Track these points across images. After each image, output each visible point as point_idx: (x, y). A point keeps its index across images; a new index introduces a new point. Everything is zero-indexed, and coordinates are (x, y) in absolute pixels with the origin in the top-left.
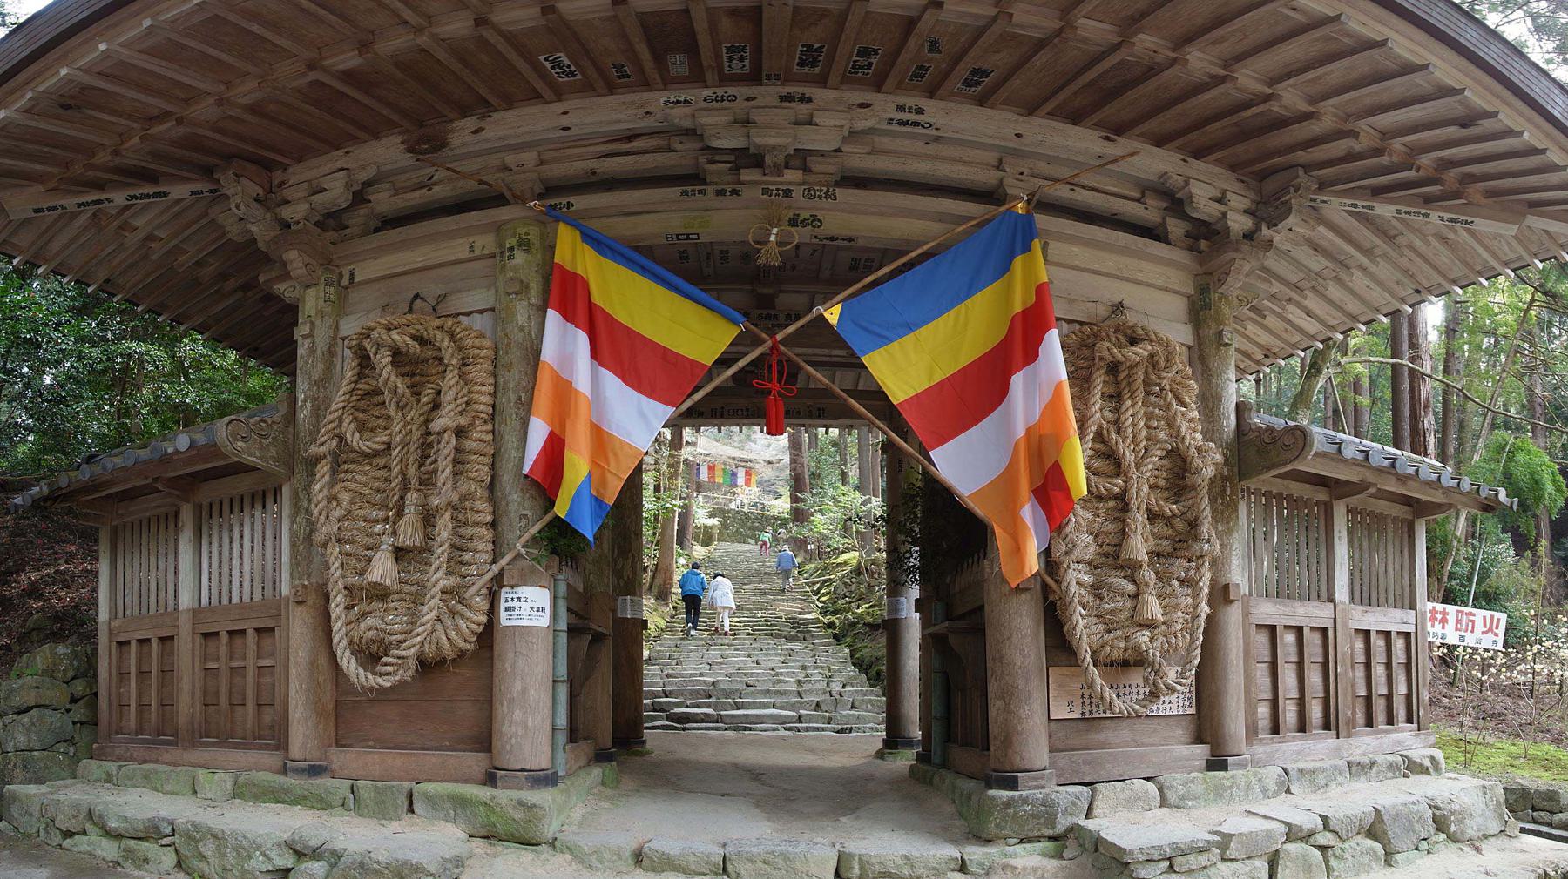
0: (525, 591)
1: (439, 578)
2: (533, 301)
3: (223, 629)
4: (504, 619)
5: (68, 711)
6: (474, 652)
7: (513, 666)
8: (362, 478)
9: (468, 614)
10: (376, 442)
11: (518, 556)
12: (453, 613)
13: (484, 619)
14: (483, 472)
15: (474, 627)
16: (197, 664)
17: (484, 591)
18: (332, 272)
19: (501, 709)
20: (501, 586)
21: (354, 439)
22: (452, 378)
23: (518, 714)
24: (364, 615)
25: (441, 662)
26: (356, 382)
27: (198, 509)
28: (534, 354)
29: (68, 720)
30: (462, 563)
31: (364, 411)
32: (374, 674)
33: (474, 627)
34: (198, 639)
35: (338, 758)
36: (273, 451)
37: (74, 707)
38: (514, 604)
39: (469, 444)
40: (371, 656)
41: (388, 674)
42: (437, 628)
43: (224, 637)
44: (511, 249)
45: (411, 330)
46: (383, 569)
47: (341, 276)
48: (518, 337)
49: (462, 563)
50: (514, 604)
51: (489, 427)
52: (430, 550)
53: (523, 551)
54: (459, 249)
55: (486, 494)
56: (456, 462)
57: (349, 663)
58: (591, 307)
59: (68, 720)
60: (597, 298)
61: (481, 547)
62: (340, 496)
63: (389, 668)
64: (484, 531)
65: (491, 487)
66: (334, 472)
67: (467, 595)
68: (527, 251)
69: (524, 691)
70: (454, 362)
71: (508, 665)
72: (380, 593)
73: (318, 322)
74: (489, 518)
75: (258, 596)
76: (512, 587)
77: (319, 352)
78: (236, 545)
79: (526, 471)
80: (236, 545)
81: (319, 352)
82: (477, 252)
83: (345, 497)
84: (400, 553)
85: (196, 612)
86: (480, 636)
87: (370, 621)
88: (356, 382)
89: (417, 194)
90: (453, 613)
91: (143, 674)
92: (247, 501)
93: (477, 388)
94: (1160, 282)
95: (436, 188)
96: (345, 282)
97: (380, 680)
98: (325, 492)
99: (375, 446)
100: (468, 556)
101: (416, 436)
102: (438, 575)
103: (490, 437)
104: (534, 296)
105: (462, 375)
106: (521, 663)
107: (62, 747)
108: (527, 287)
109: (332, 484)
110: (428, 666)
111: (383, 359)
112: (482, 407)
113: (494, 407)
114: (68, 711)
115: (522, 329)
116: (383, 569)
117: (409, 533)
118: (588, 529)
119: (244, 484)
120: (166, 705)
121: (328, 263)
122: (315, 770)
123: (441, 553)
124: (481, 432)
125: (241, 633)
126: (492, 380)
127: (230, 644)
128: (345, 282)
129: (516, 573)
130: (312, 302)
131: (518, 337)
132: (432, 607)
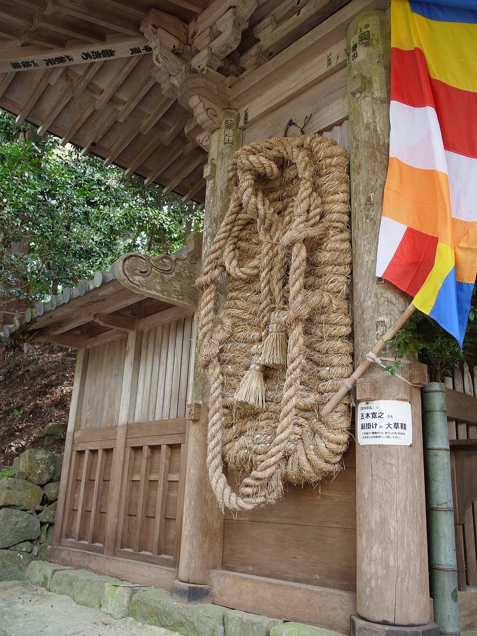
0: (382, 406)
1: (291, 394)
2: (377, 94)
3: (145, 443)
4: (363, 439)
5: (38, 512)
6: (340, 473)
7: (371, 492)
8: (242, 303)
9: (326, 433)
10: (247, 270)
11: (372, 366)
12: (315, 432)
13: (344, 437)
14: (340, 283)
15: (334, 446)
16: (126, 476)
17: (342, 408)
18: (231, 115)
19: (362, 542)
20: (358, 402)
21: (232, 267)
22: (304, 190)
23: (377, 550)
24: (241, 433)
25: (308, 485)
26: (237, 213)
27: (140, 335)
28: (381, 150)
29: (36, 520)
30: (321, 379)
31: (247, 240)
32: (238, 495)
33: (334, 446)
34: (128, 450)
35: (223, 582)
36: (177, 285)
37: (45, 508)
38: (370, 420)
39: (324, 256)
40: (234, 473)
41: (248, 496)
42: (316, 455)
43: (146, 451)
44: (355, 47)
45: (273, 153)
46: (250, 388)
47: (238, 117)
48: (364, 136)
49: (321, 379)
50: (370, 420)
51: (345, 235)
52: (284, 367)
53: (378, 360)
54: (318, 66)
55: (344, 305)
56: (308, 274)
57: (218, 482)
58: (432, 83)
59: (36, 520)
60: (436, 75)
61: (336, 360)
62: (224, 320)
63: (249, 490)
64: (339, 343)
65: (350, 297)
66: (216, 299)
67: (323, 412)
68: (367, 45)
69: (383, 522)
70: (307, 174)
71: (365, 490)
72: (248, 413)
73: (219, 164)
74: (345, 330)
75: (173, 415)
76: (367, 401)
77: (219, 192)
78: (162, 368)
79: (380, 273)
80: (162, 368)
81: (219, 192)
82: (334, 64)
83: (228, 322)
84: (268, 373)
85: (129, 427)
86: (345, 455)
87: (242, 440)
88: (237, 213)
89: (290, 21)
90: (315, 432)
91: (90, 481)
92: (173, 327)
93: (330, 198)
94: (174, 34)
95: (303, 11)
96: (241, 123)
97: (241, 502)
98: (211, 315)
99: (248, 271)
100: (324, 372)
101: (280, 256)
102: (291, 391)
103: (346, 245)
104: (378, 89)
105: (316, 188)
106: (378, 488)
107: (25, 547)
108: (370, 82)
109: (216, 310)
110: (296, 489)
111: (246, 181)
112: (335, 216)
113: (350, 214)
114: (38, 512)
115: (367, 127)
116: (250, 388)
117: (266, 359)
118: (455, 329)
119: (169, 316)
120: (100, 523)
121: (228, 107)
122: (196, 594)
123: (293, 374)
124: (335, 242)
125: (158, 448)
126: (344, 187)
127: (150, 458)
128: (241, 123)
129: (367, 386)
130: (215, 144)
131: (364, 136)
132: (287, 429)
